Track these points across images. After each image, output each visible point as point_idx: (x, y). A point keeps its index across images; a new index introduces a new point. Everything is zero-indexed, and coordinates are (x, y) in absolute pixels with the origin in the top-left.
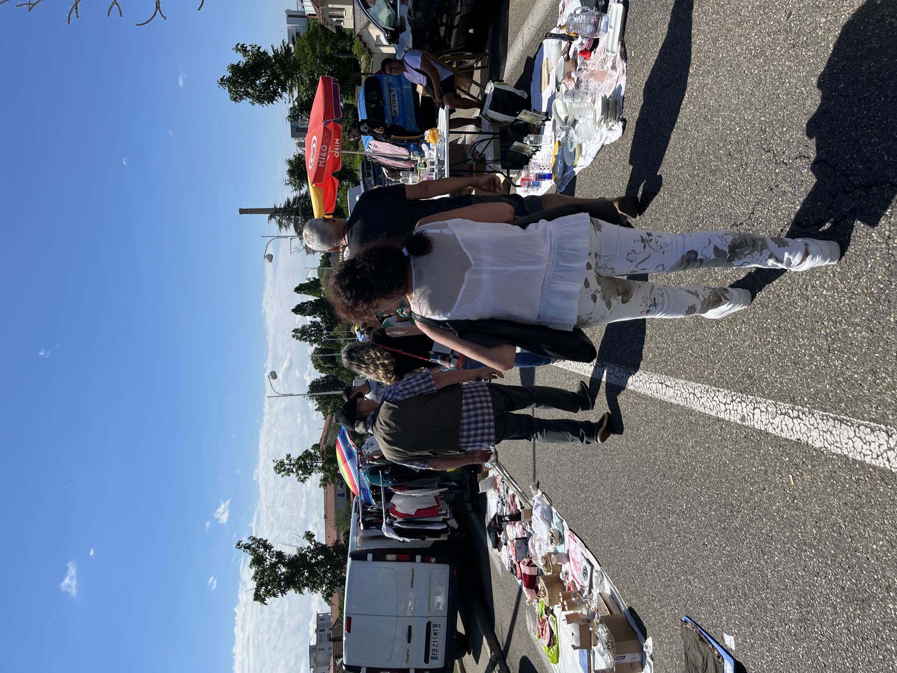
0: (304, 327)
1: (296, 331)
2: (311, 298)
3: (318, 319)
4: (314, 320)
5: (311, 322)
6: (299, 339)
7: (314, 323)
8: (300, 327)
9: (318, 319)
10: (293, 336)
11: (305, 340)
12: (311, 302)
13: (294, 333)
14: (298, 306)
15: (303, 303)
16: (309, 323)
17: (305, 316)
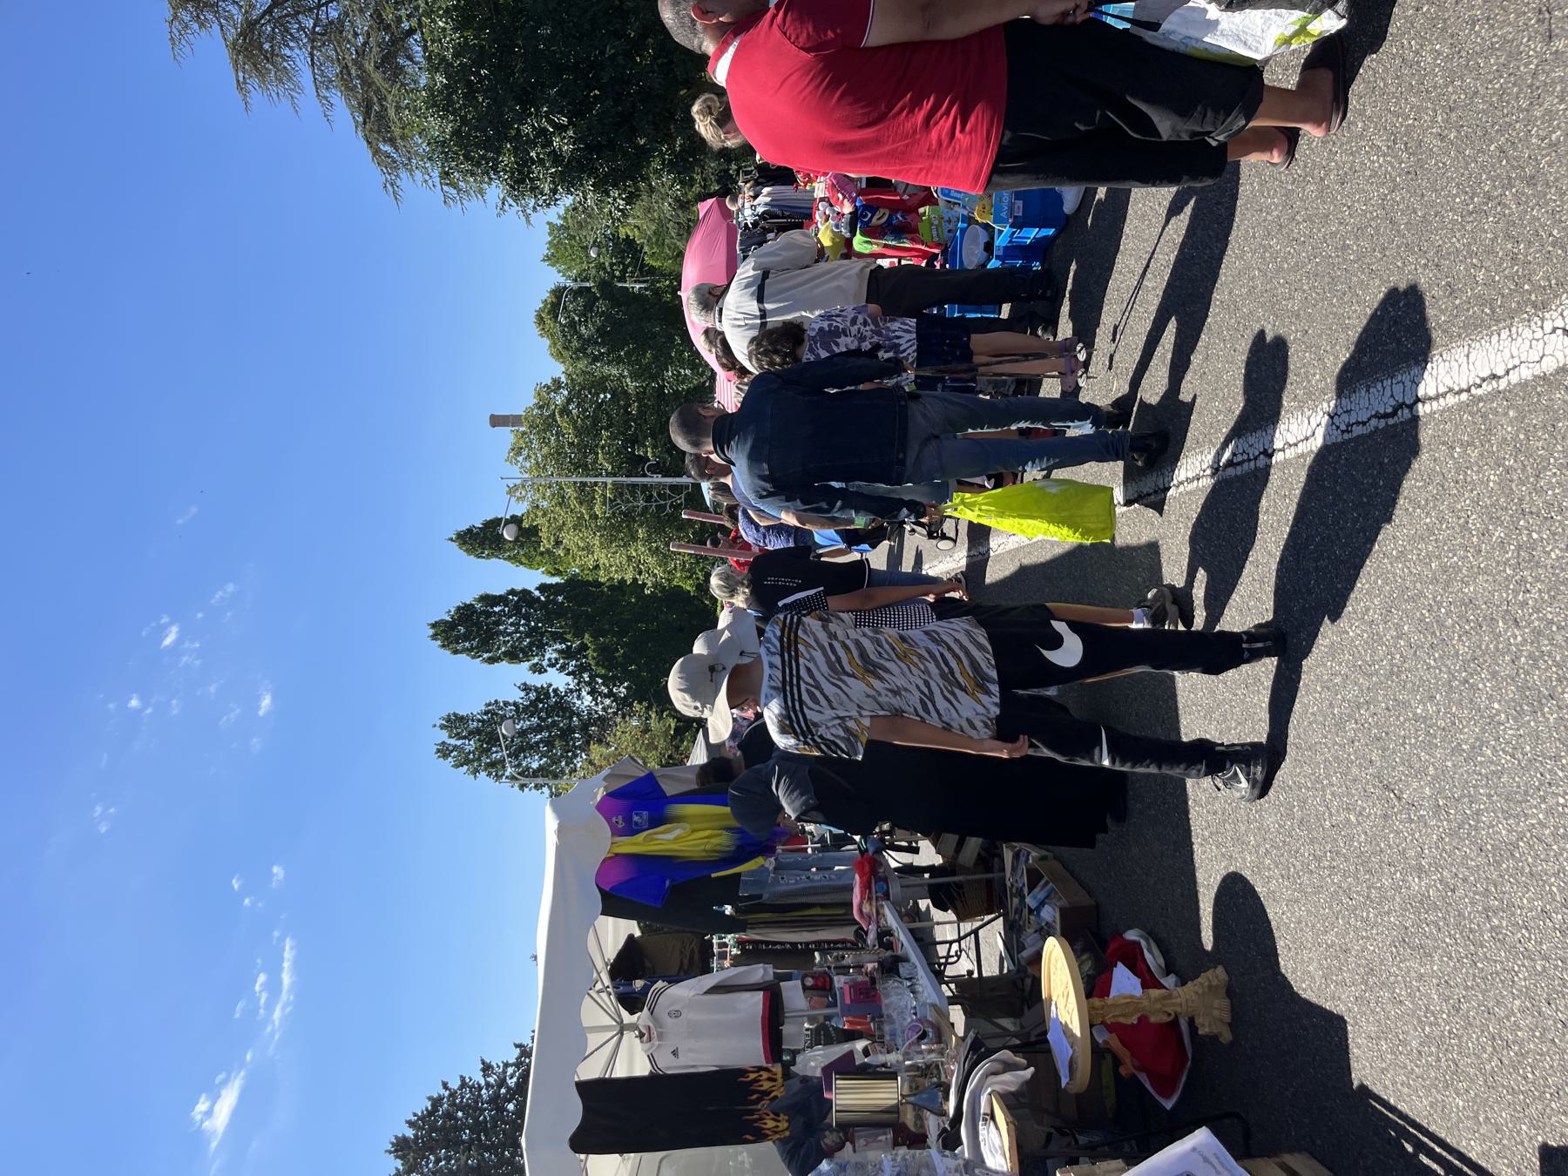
1: (455, 723)
2: (531, 579)
3: (558, 680)
4: (538, 680)
5: (526, 688)
6: (467, 762)
7: (543, 693)
8: (473, 707)
10: (444, 751)
11: (495, 768)
12: (525, 593)
13: (443, 736)
14: (465, 614)
16: (517, 696)
17: (492, 660)
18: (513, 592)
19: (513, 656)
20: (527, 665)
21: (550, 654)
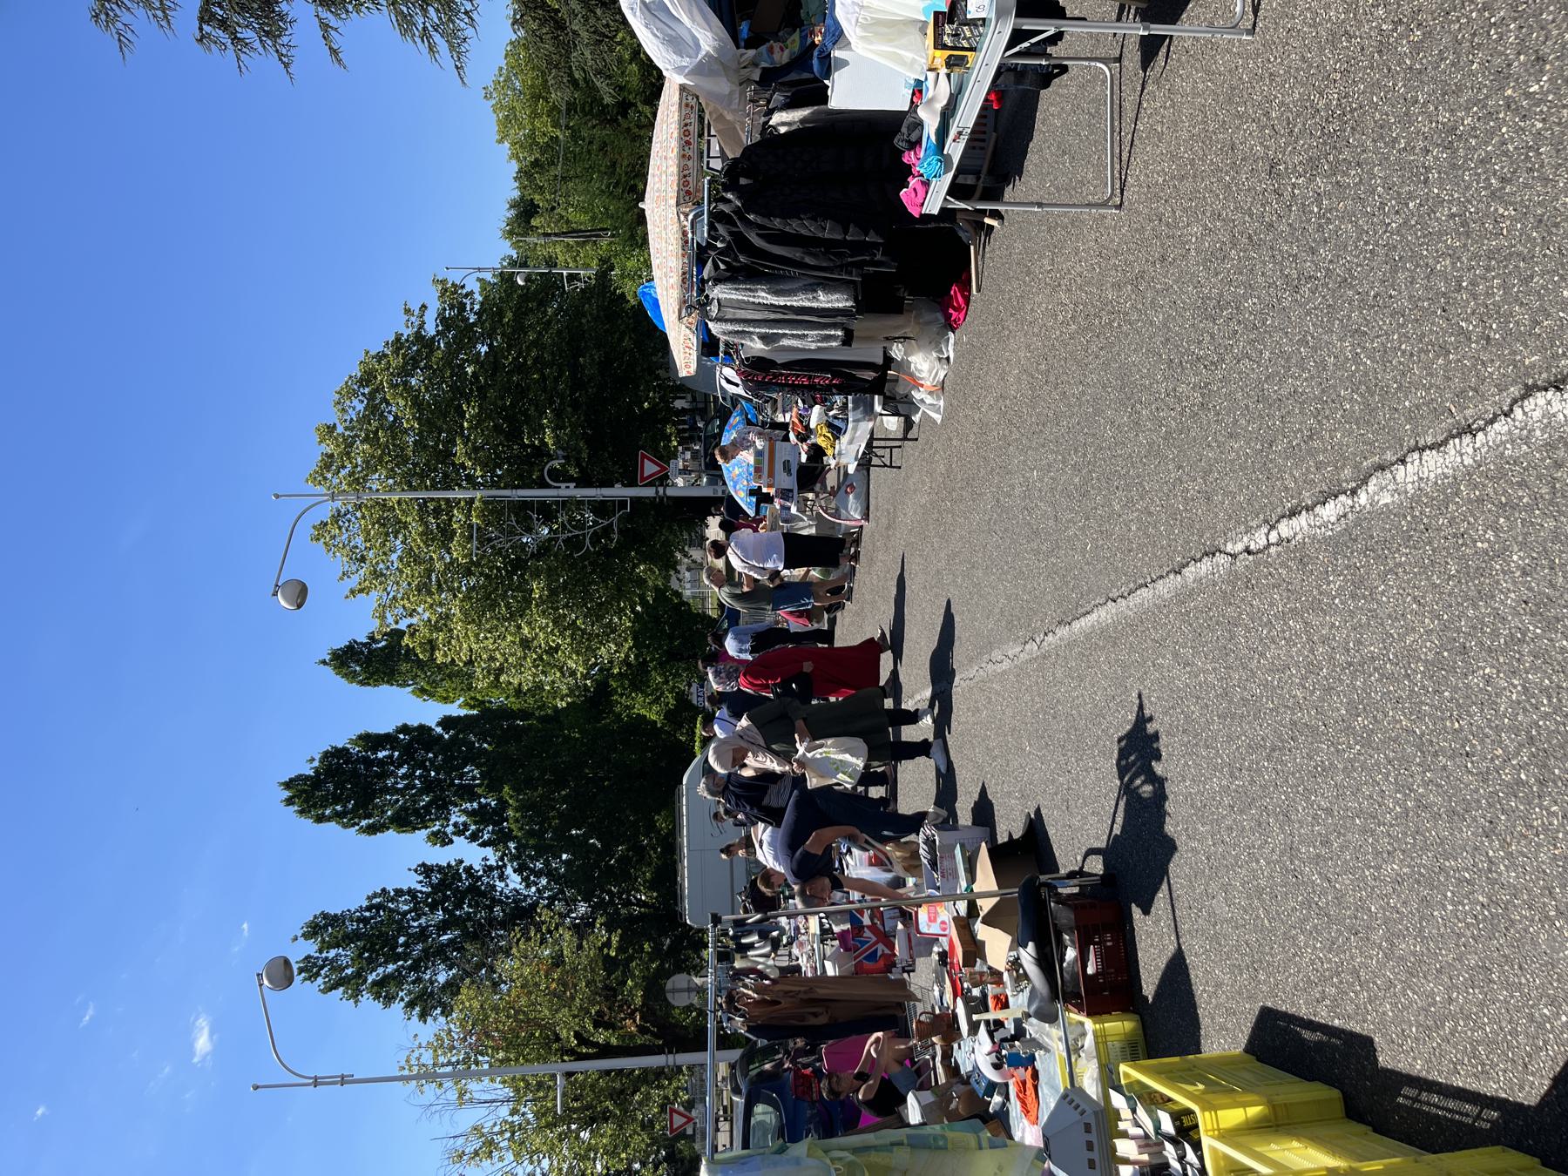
0: (382, 902)
3: (471, 854)
4: (442, 856)
5: (426, 870)
8: (349, 898)
9: (471, 854)
11: (384, 991)
12: (423, 729)
14: (336, 761)
15: (372, 741)
16: (413, 881)
17: (372, 830)
18: (405, 729)
19: (405, 821)
20: (424, 833)
21: (457, 817)
